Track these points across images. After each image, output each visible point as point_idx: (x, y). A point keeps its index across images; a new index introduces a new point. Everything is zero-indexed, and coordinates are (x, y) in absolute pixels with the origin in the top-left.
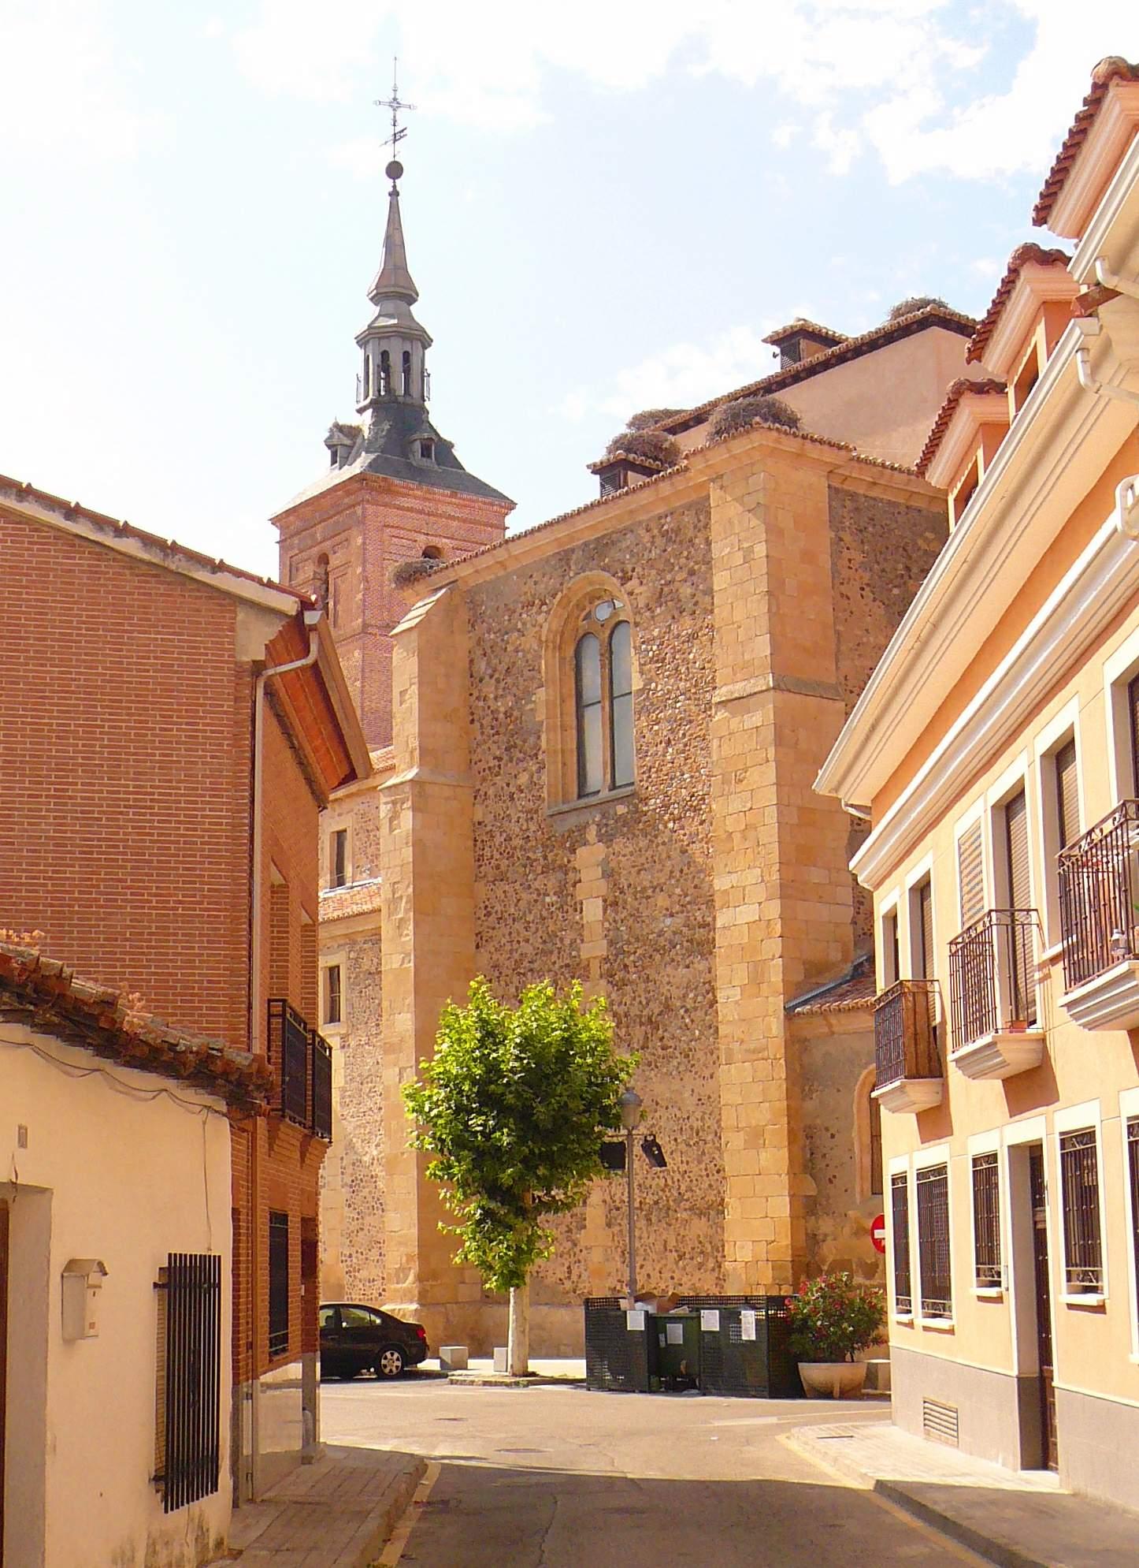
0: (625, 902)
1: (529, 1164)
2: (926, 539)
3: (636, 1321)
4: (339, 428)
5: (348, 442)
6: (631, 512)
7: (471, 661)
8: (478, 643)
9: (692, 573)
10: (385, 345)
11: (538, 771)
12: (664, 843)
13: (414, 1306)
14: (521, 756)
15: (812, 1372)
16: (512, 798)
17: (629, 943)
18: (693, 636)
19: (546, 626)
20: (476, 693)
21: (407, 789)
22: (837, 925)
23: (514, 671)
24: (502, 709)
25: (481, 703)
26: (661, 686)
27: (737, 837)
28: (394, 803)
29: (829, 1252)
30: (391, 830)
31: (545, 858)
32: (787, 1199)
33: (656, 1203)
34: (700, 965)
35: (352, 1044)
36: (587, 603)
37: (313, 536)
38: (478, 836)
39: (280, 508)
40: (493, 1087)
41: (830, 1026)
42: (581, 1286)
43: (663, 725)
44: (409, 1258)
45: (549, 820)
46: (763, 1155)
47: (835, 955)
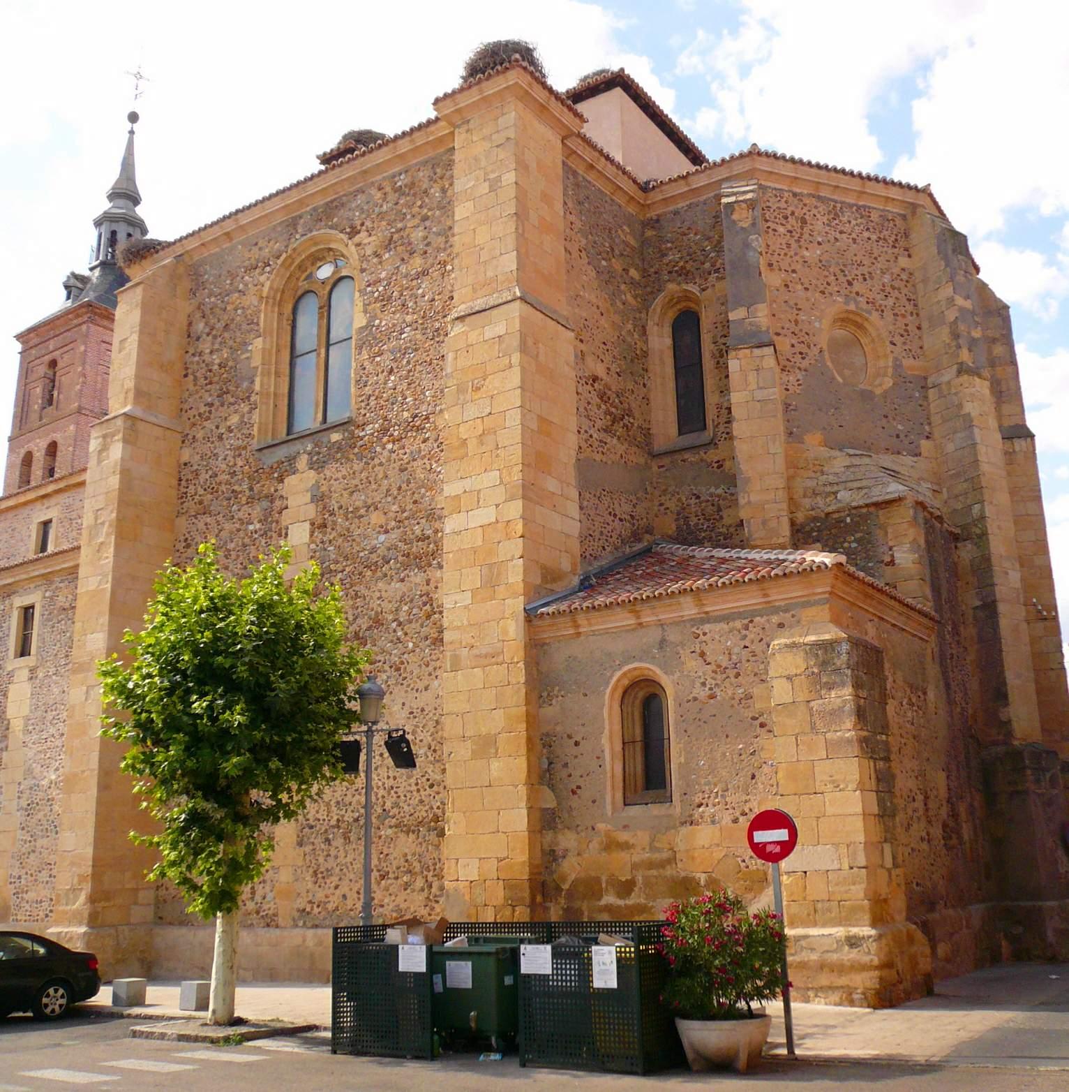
0: (335, 523)
1: (260, 753)
2: (623, 231)
3: (412, 958)
4: (75, 276)
5: (80, 285)
6: (365, 172)
7: (190, 324)
8: (199, 308)
9: (425, 218)
10: (114, 227)
11: (250, 412)
12: (381, 464)
13: (83, 929)
14: (232, 400)
15: (701, 1034)
16: (220, 438)
17: (337, 562)
18: (425, 273)
19: (268, 284)
20: (191, 351)
21: (119, 422)
22: (568, 536)
23: (232, 326)
24: (217, 361)
25: (197, 358)
26: (384, 321)
27: (472, 445)
28: (104, 437)
29: (571, 869)
30: (99, 462)
31: (251, 489)
32: (525, 812)
33: (357, 820)
34: (417, 577)
35: (41, 675)
36: (309, 264)
37: (47, 347)
38: (183, 476)
39: (22, 328)
40: (220, 659)
41: (577, 626)
42: (265, 907)
43: (385, 356)
44: (82, 879)
45: (257, 455)
46: (495, 765)
47: (566, 565)
